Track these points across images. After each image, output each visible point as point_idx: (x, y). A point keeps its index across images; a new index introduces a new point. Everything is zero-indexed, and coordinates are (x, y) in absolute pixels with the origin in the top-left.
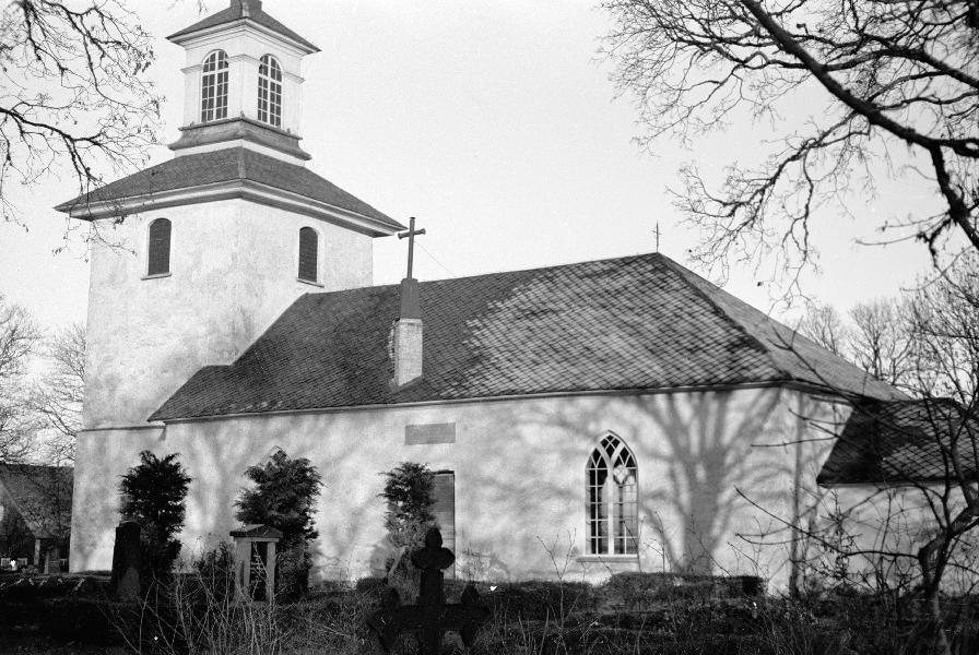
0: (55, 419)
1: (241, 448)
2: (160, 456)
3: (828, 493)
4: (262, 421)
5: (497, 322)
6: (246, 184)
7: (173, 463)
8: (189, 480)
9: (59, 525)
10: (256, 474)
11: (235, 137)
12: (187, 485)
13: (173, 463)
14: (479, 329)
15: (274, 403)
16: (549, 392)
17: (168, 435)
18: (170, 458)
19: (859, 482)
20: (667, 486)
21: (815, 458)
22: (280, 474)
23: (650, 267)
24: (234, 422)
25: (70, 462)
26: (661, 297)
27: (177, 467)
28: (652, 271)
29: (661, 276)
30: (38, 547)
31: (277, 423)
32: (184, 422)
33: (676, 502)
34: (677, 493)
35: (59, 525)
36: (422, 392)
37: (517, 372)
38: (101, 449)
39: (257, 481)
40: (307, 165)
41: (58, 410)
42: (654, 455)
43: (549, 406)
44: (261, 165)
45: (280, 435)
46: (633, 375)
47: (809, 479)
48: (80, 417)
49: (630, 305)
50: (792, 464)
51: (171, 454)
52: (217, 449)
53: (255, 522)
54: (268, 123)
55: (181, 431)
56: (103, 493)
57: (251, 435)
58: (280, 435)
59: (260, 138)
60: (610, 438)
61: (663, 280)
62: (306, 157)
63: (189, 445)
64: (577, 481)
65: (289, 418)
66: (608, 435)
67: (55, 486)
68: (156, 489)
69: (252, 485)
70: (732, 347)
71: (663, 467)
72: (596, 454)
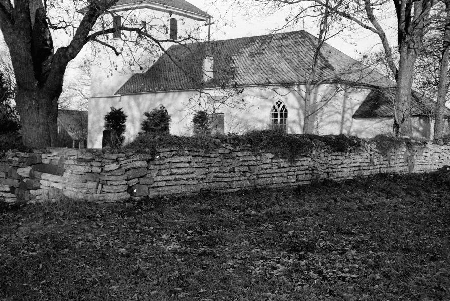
1: (147, 104)
2: (117, 109)
3: (356, 121)
4: (154, 94)
5: (242, 57)
7: (121, 111)
8: (127, 117)
9: (83, 134)
10: (147, 115)
12: (126, 118)
13: (121, 111)
14: (235, 60)
15: (160, 88)
16: (257, 85)
17: (122, 100)
18: (120, 109)
19: (364, 117)
20: (296, 118)
21: (352, 109)
22: (155, 115)
23: (300, 36)
24: (144, 95)
25: (86, 110)
26: (300, 48)
27: (122, 112)
28: (300, 38)
29: (304, 40)
30: (74, 144)
31: (160, 95)
32: (127, 95)
33: (300, 124)
34: (300, 121)
35: (83, 134)
36: (214, 83)
37: (247, 77)
38: (97, 105)
41: (81, 89)
42: (292, 107)
43: (256, 90)
45: (161, 100)
46: (286, 78)
47: (348, 116)
48: (89, 92)
49: (290, 51)
50: (341, 110)
51: (121, 108)
52: (138, 105)
53: (144, 130)
55: (125, 98)
56: (98, 121)
57: (151, 100)
58: (161, 100)
60: (279, 101)
61: (303, 41)
63: (128, 104)
64: (266, 117)
65: (164, 94)
66: (278, 100)
68: (116, 120)
69: (146, 118)
71: (295, 112)
72: (274, 107)
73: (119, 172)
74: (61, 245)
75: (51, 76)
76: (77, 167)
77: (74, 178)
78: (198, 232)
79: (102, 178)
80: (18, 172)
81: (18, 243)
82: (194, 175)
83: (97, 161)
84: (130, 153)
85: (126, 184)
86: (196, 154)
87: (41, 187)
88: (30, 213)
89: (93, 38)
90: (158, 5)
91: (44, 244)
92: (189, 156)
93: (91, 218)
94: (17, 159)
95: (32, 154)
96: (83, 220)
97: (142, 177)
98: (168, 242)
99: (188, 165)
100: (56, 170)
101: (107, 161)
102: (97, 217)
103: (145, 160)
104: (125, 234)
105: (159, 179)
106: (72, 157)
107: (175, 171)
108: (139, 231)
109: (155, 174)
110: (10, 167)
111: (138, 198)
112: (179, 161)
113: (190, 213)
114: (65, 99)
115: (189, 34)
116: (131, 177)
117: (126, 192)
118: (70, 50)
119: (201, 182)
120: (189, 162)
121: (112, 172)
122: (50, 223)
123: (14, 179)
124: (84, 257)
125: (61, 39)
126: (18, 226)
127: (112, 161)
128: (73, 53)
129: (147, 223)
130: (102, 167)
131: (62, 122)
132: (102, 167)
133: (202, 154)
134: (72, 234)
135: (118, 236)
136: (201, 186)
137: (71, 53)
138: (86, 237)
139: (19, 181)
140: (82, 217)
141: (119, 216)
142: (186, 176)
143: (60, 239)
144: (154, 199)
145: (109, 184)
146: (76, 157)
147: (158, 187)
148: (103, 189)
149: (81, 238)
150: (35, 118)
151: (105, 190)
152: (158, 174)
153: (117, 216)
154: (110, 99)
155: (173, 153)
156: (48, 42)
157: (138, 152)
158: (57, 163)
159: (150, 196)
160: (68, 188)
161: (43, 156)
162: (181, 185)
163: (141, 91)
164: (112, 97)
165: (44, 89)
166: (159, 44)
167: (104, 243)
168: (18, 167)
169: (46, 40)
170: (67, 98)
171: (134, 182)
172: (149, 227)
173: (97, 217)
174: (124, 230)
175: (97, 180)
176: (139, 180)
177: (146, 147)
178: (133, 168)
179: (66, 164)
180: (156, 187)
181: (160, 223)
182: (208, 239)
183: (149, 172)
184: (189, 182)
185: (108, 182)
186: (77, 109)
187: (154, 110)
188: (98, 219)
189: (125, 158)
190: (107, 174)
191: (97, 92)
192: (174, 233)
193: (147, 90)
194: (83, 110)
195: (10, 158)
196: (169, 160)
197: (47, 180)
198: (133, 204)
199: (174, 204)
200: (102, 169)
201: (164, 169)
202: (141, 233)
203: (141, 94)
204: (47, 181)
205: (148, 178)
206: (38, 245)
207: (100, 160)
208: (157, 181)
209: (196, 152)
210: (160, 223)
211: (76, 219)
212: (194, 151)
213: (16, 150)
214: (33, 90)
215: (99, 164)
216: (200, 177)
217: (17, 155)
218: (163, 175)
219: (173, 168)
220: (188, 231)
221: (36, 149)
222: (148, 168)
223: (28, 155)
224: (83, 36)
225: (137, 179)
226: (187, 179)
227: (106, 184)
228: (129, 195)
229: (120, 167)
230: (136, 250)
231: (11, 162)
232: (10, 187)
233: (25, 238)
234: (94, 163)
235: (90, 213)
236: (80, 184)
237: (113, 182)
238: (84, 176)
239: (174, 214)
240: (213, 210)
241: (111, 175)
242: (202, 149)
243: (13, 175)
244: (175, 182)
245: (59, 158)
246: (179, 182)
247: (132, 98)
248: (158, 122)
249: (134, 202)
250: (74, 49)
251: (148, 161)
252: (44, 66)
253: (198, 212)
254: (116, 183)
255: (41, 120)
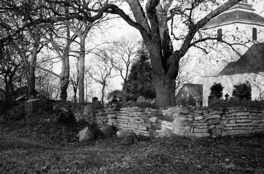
0: (199, 74)
2: (218, 83)
4: (241, 74)
6: (238, 20)
8: (223, 88)
10: (235, 86)
11: (236, 8)
12: (223, 89)
13: (220, 84)
15: (245, 70)
18: (219, 83)
22: (240, 86)
24: (236, 75)
25: (202, 84)
38: (208, 81)
39: (236, 88)
40: (254, 12)
41: (199, 72)
44: (242, 14)
45: (246, 77)
51: (220, 82)
52: (232, 81)
54: (244, 3)
57: (240, 77)
59: (242, 7)
62: (254, 10)
63: (226, 80)
67: (199, 88)
69: (235, 88)
70: (209, 34)
73: (203, 121)
74: (165, 161)
75: (171, 66)
76: (180, 118)
77: (178, 124)
78: (248, 158)
79: (194, 124)
80: (150, 119)
81: (143, 158)
82: (251, 124)
83: (190, 114)
84: (210, 110)
85: (208, 128)
86: (252, 111)
87: (162, 128)
88: (154, 142)
89: (193, 44)
90: (245, 21)
91: (156, 160)
92: (247, 112)
93: (185, 147)
94: (150, 112)
95: (157, 110)
96: (181, 148)
97: (217, 124)
98: (228, 163)
99: (247, 117)
100: (170, 119)
101: (196, 114)
102: (189, 147)
103: (219, 114)
104: (203, 157)
105: (228, 126)
106: (177, 112)
107: (238, 121)
108: (212, 156)
109: (225, 122)
110: (146, 117)
111: (214, 136)
112: (241, 115)
113: (245, 146)
114: (190, 78)
115: (249, 39)
116: (210, 124)
117: (207, 133)
118: (181, 52)
119: (256, 128)
120: (248, 116)
121: (199, 121)
122: (163, 149)
123: (148, 123)
124: (176, 168)
125: (177, 45)
126: (146, 149)
127: (199, 114)
128: (182, 53)
129: (217, 151)
130: (193, 118)
131: (190, 91)
132: (193, 118)
133: (256, 111)
134: (173, 155)
135: (199, 158)
136: (255, 130)
137: (181, 54)
138: (180, 157)
139: (151, 125)
140: (181, 146)
141: (202, 146)
142: (245, 124)
143: (166, 158)
144: (224, 137)
145: (197, 128)
146: (179, 112)
147: (228, 130)
148: (194, 131)
149: (177, 158)
150: (163, 90)
151: (195, 131)
152: (227, 123)
153: (201, 146)
154: (215, 77)
155: (237, 110)
156: (170, 48)
157: (215, 110)
158: (170, 115)
159: (222, 135)
160: (175, 129)
161: (163, 111)
162: (242, 129)
163: (234, 72)
164: (217, 76)
165: (168, 74)
166: (231, 46)
167: (190, 162)
168: (150, 117)
169: (169, 47)
170: (191, 77)
171: (212, 127)
172: (218, 154)
173: (189, 147)
174: (203, 155)
175: (191, 125)
176: (215, 126)
177: (220, 106)
178: (212, 119)
179: (174, 116)
180: (226, 130)
181: (225, 152)
182: (253, 162)
183: (221, 121)
184: (247, 128)
185: (197, 126)
186: (197, 83)
187: (240, 83)
188: (189, 148)
189: (207, 113)
190: (196, 122)
191: (208, 74)
192: (233, 158)
193: (237, 71)
194: (201, 84)
195: (146, 112)
196: (234, 114)
197: (165, 124)
198: (212, 139)
199: (237, 141)
200: (193, 119)
201: (231, 120)
202: (213, 157)
203: (234, 74)
204: (165, 125)
205: (221, 125)
206: (153, 160)
207: (192, 114)
208: (227, 127)
209: (252, 109)
210: (225, 152)
211: (177, 147)
212: (250, 109)
213: (151, 108)
214: (161, 75)
215: (192, 116)
216: (254, 125)
217: (150, 110)
218: (230, 123)
219: (237, 119)
220: (242, 158)
221: (161, 107)
222: (221, 119)
223: (155, 111)
224: (188, 44)
225: (214, 125)
226: (246, 126)
227: (196, 128)
228: (209, 134)
229: (204, 118)
230: (207, 166)
231: (147, 114)
232: (147, 128)
233: (147, 156)
234: (189, 116)
235: (185, 144)
236: (181, 127)
237: (200, 127)
238: (183, 122)
239: (235, 147)
240: (261, 145)
241: (199, 122)
242: (256, 108)
243: (148, 121)
244: (239, 128)
245: (171, 112)
246: (241, 128)
247: (228, 76)
248: (243, 91)
249: (212, 138)
250: (183, 51)
251: (221, 115)
252: (168, 61)
253: (251, 146)
254: (201, 127)
255: (166, 91)
